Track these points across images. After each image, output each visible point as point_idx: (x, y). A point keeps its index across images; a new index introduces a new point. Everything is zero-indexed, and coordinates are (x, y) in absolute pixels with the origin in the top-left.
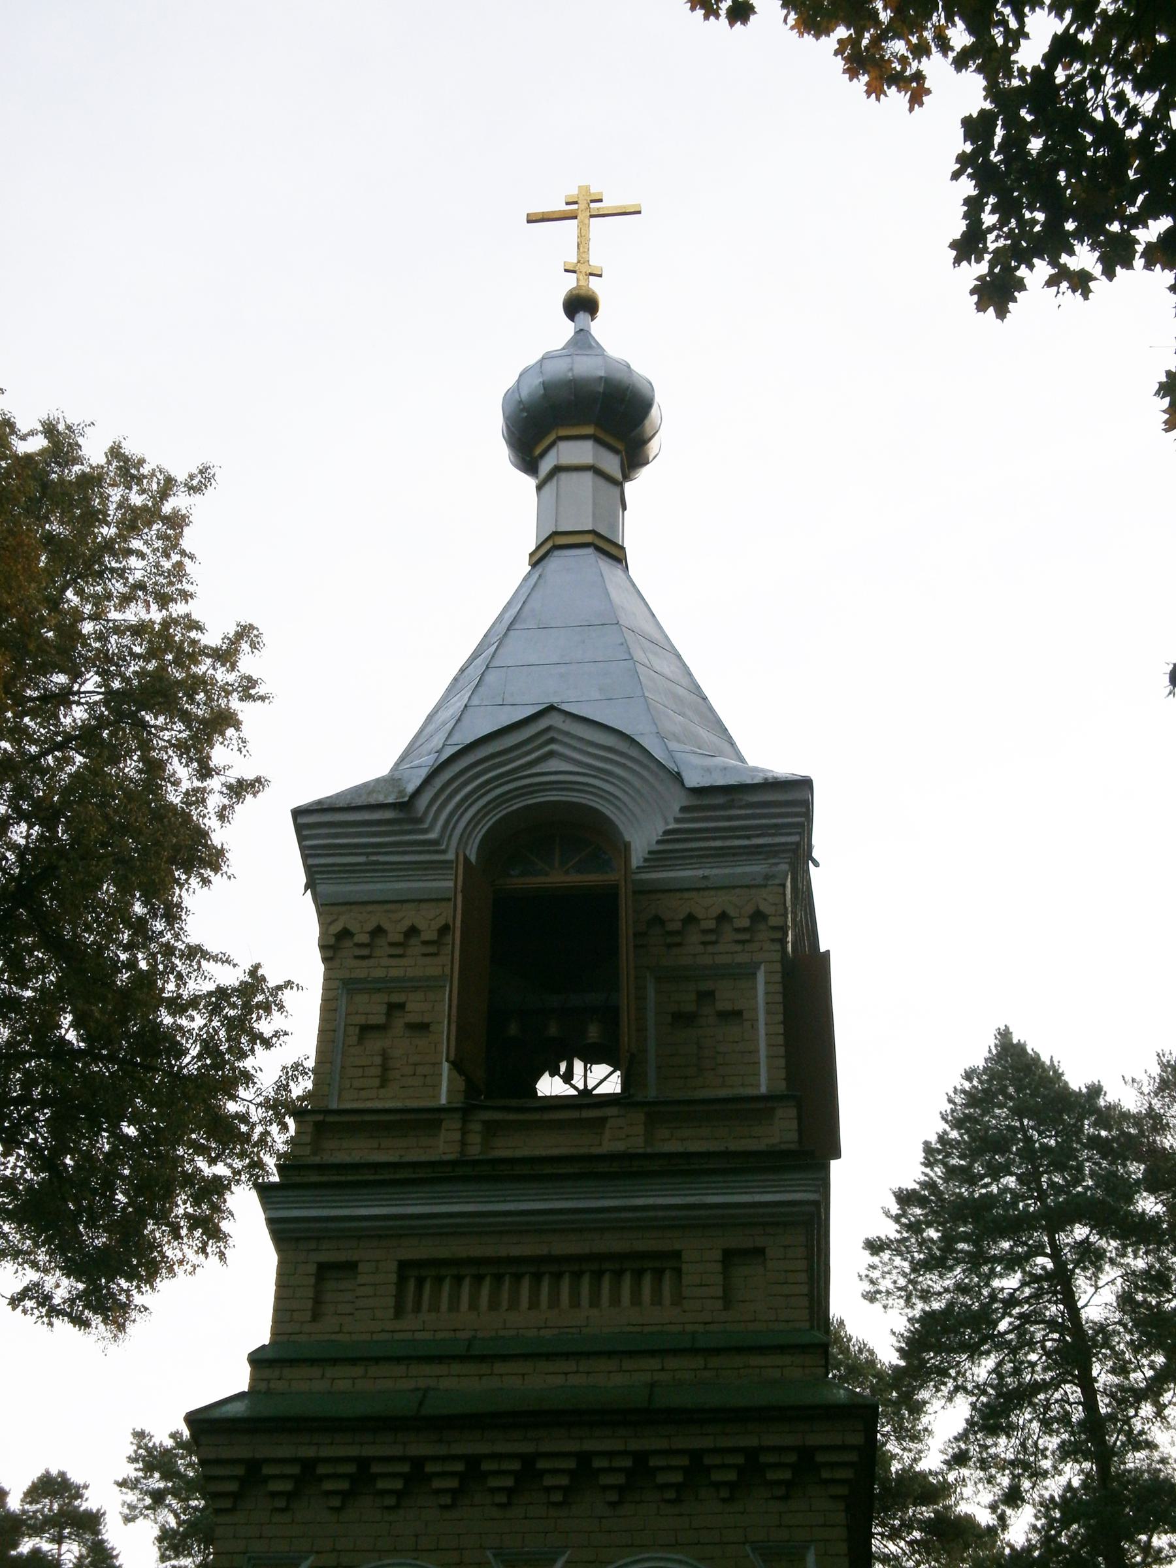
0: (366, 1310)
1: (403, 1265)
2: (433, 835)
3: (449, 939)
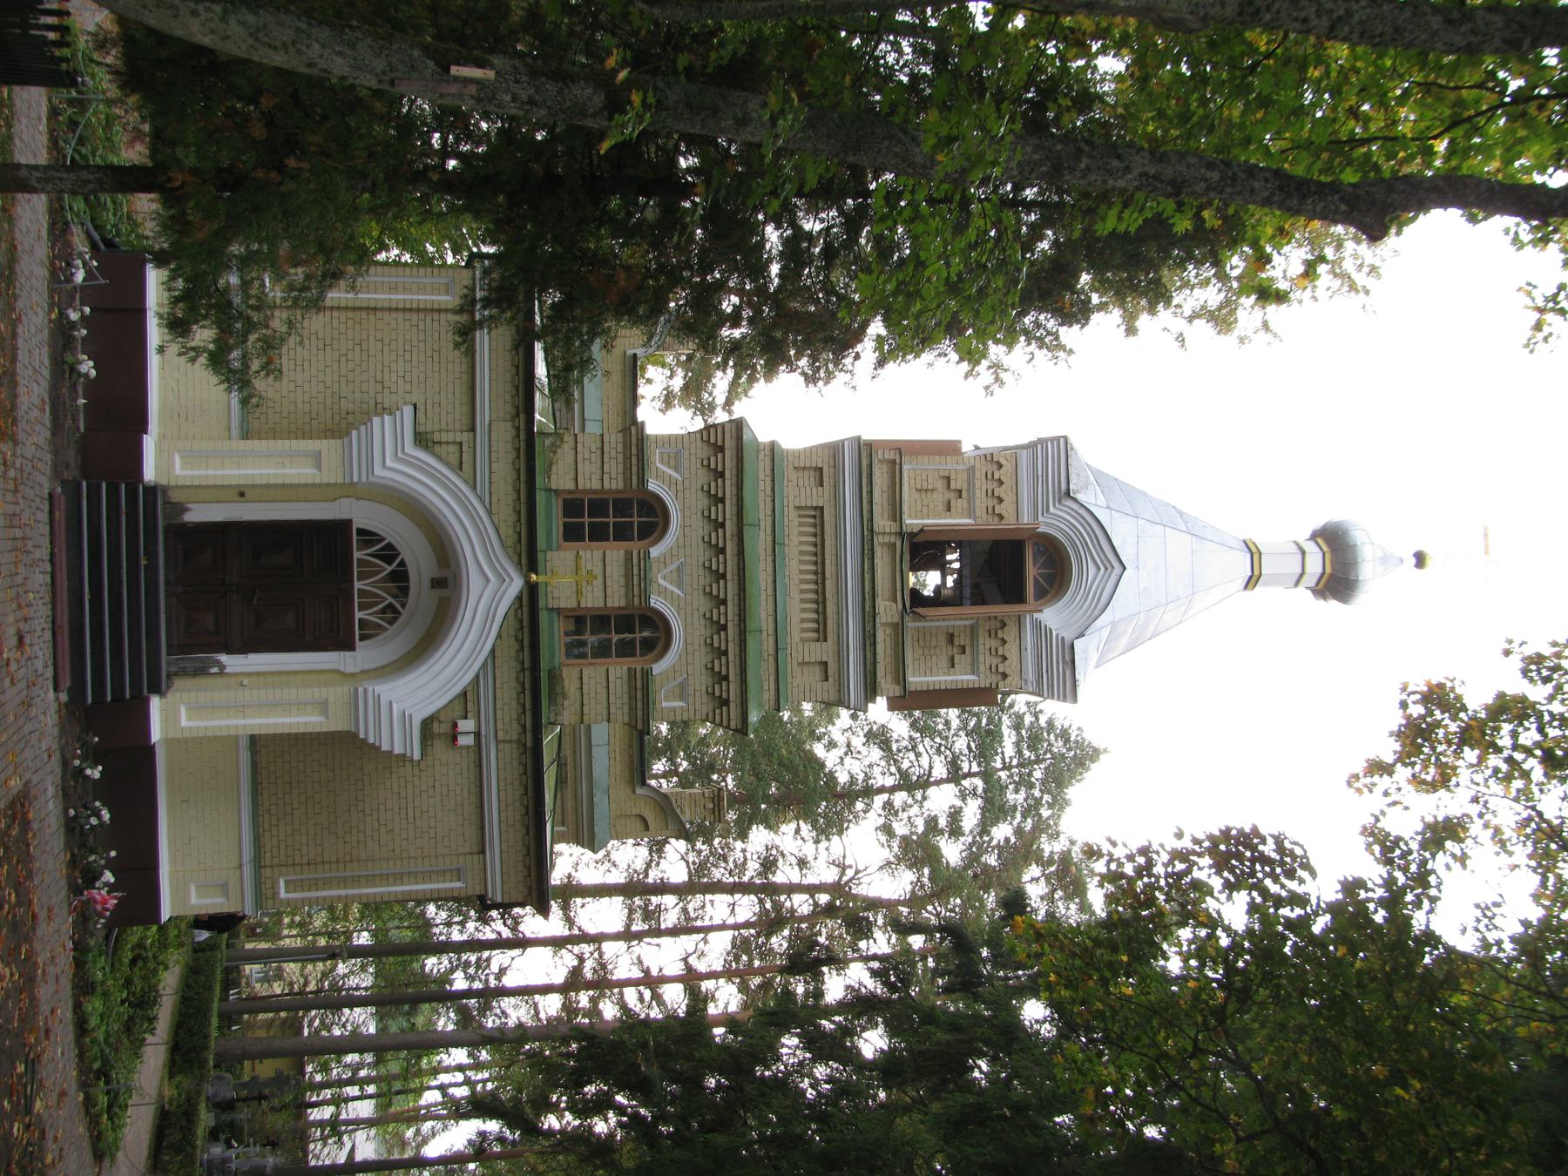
0: (799, 492)
1: (822, 508)
2: (1052, 509)
3: (996, 519)
